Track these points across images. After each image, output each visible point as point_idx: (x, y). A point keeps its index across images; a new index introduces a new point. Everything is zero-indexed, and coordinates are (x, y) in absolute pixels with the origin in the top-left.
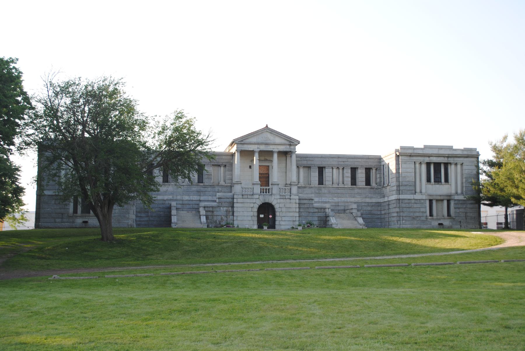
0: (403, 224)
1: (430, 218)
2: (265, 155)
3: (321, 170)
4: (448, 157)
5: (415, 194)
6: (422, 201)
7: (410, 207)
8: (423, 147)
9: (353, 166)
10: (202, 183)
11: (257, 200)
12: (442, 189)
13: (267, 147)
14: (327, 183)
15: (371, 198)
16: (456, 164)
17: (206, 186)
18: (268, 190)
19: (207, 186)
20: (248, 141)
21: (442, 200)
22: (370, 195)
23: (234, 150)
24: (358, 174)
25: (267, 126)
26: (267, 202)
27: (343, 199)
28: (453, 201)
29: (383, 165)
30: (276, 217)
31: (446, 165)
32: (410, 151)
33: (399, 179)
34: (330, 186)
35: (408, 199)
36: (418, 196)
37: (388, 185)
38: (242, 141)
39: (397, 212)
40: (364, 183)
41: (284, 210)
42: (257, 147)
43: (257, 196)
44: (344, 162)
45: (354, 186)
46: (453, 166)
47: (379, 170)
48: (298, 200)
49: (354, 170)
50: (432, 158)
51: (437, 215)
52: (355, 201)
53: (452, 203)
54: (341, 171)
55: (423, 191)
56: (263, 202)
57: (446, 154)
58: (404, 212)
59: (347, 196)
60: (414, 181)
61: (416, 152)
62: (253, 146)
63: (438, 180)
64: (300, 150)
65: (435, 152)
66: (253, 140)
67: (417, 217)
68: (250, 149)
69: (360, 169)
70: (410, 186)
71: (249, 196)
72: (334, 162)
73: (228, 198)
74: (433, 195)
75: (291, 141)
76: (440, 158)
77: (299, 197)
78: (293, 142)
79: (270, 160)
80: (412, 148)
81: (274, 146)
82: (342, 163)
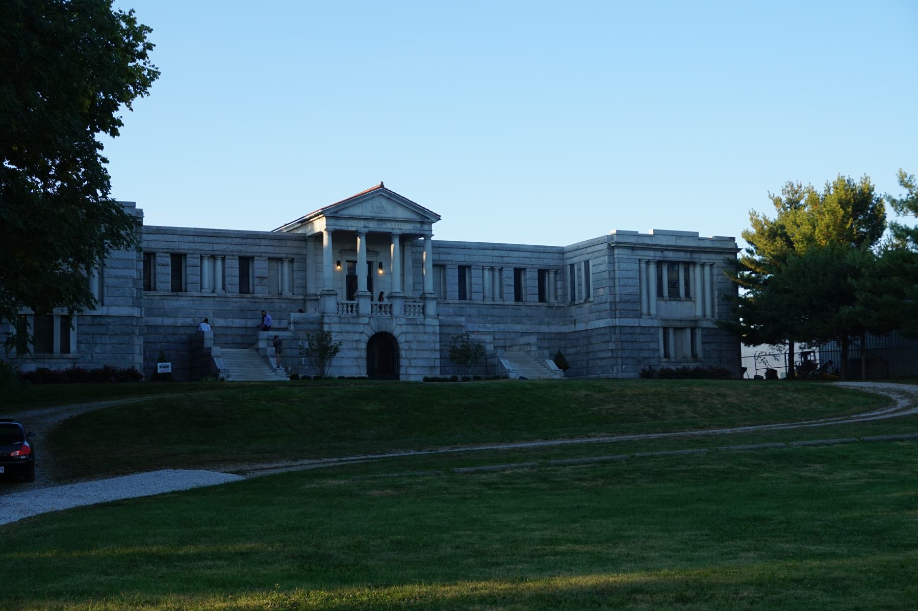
0: (622, 372)
1: (664, 360)
2: (378, 240)
3: (463, 270)
4: (692, 252)
5: (641, 318)
6: (653, 331)
7: (634, 342)
8: (651, 233)
9: (518, 266)
10: (248, 292)
11: (366, 326)
12: (680, 310)
13: (381, 225)
14: (474, 296)
15: (549, 324)
16: (703, 265)
17: (257, 300)
18: (349, 306)
19: (260, 300)
20: (345, 213)
21: (682, 329)
22: (546, 319)
23: (320, 225)
24: (525, 280)
25: (382, 185)
26: (384, 330)
27: (502, 327)
28: (700, 329)
29: (572, 266)
30: (401, 360)
31: (688, 265)
32: (633, 240)
33: (615, 291)
34: (480, 302)
35: (631, 327)
36: (645, 322)
37: (586, 301)
38: (336, 212)
39: (612, 350)
40: (536, 298)
41: (414, 346)
42: (363, 225)
43: (366, 320)
44: (502, 257)
45: (520, 303)
46: (698, 269)
47: (560, 273)
48: (438, 327)
49: (518, 272)
50: (666, 253)
51: (676, 357)
52: (522, 329)
53: (699, 333)
54: (497, 274)
55: (653, 311)
56: (377, 330)
57: (690, 247)
58: (624, 350)
59: (509, 321)
60: (639, 293)
61: (641, 241)
62: (356, 222)
63: (674, 294)
64: (440, 232)
65: (672, 242)
66: (356, 211)
67: (645, 358)
68: (350, 229)
69: (530, 271)
70: (634, 302)
71: (351, 319)
72: (487, 258)
73: (311, 323)
74: (669, 320)
75: (426, 215)
76: (679, 253)
77: (440, 322)
78: (427, 218)
79: (373, 251)
80: (635, 234)
81: (393, 224)
82: (499, 260)
